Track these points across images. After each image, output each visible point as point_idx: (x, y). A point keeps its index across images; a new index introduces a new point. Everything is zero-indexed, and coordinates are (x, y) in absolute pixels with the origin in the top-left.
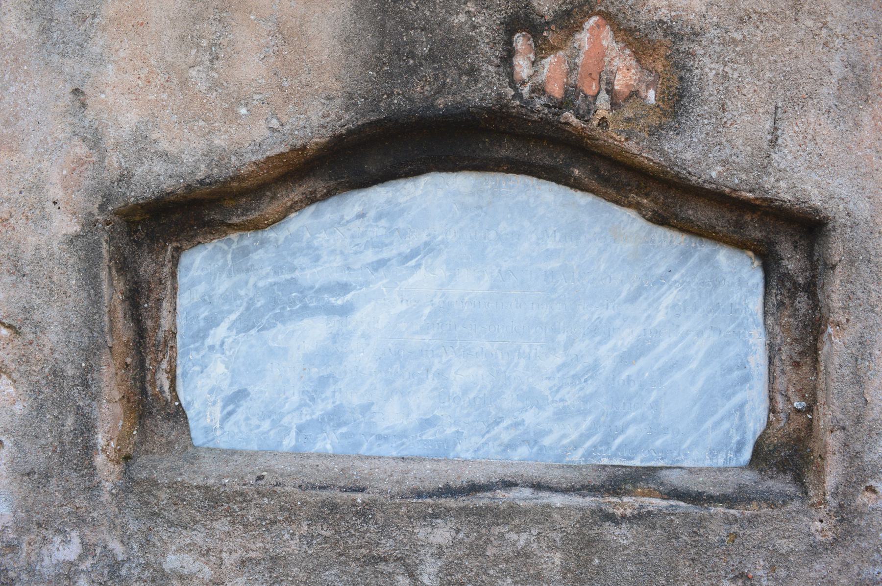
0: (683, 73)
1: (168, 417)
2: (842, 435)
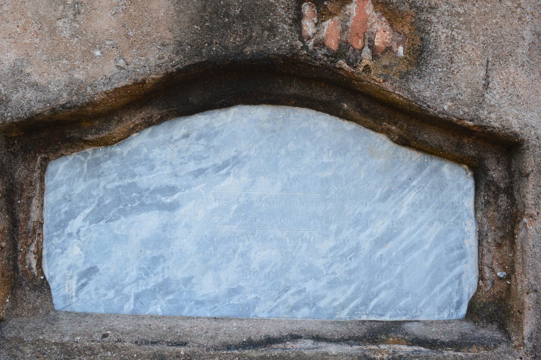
0: (423, 35)
1: (35, 288)
2: (535, 295)
